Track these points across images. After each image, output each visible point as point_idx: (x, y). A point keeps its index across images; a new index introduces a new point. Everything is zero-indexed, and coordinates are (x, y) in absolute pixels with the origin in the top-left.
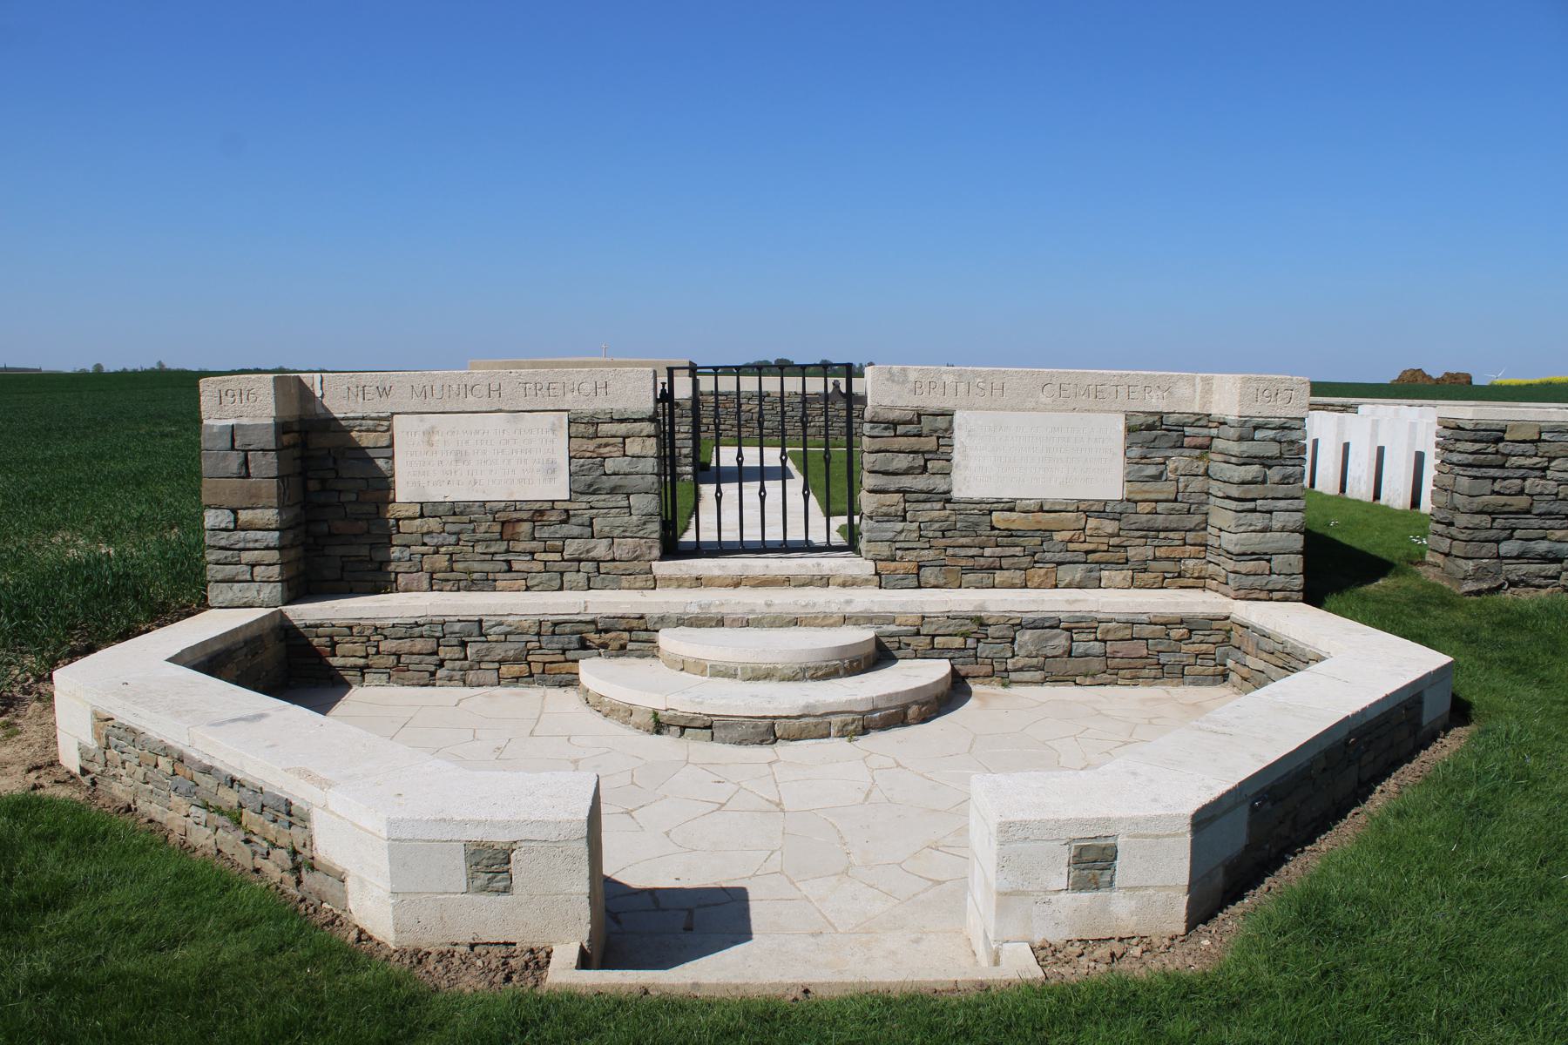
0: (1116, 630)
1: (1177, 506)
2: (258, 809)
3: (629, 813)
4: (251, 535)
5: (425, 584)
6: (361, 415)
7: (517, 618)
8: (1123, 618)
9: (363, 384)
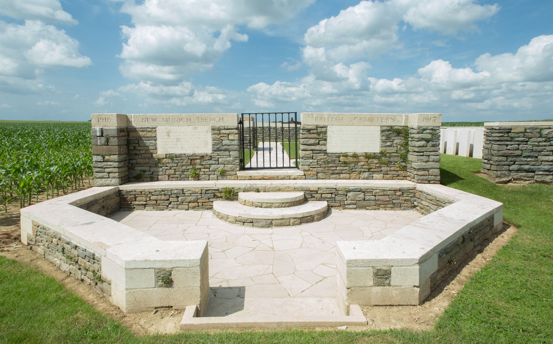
0: (379, 192)
2: (84, 257)
3: (224, 251)
4: (109, 163)
5: (167, 178)
9: (147, 117)
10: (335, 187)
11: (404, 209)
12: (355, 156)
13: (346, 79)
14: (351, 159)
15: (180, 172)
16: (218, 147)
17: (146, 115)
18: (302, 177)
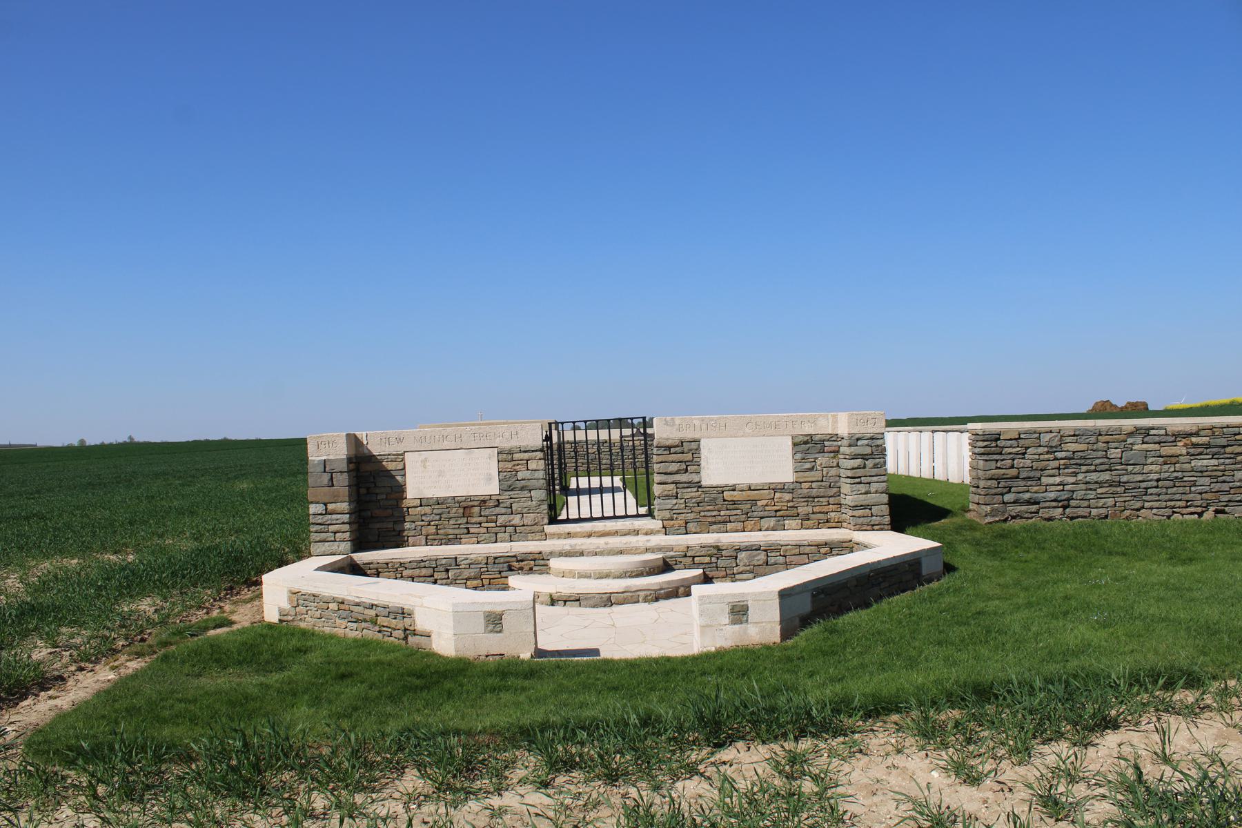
0: (790, 549)
1: (823, 484)
4: (334, 516)
5: (424, 542)
7: (475, 556)
8: (794, 543)
16: (509, 483)
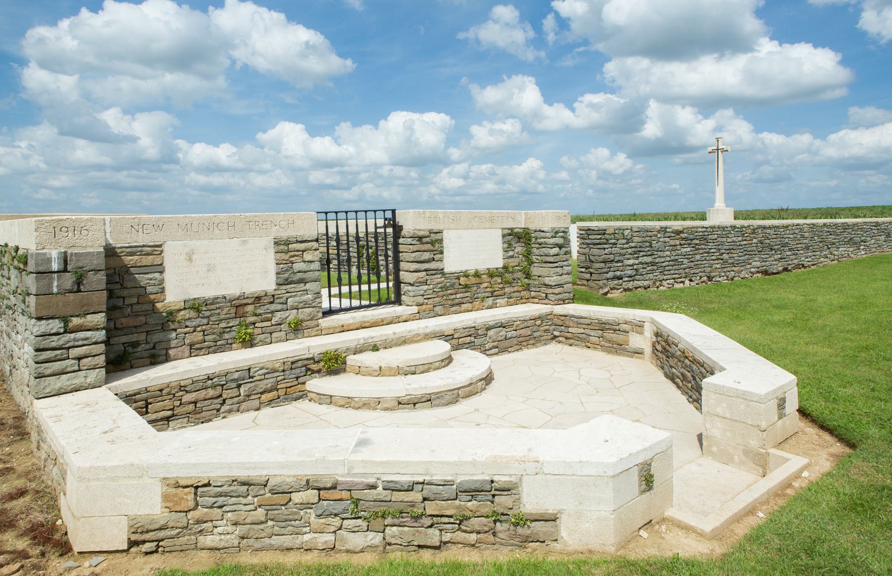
5: (187, 353)
6: (142, 244)
9: (143, 223)
10: (473, 325)
11: (545, 344)
12: (477, 275)
13: (133, 139)
14: (473, 280)
15: (214, 336)
17: (140, 219)
18: (415, 316)
